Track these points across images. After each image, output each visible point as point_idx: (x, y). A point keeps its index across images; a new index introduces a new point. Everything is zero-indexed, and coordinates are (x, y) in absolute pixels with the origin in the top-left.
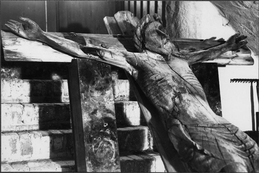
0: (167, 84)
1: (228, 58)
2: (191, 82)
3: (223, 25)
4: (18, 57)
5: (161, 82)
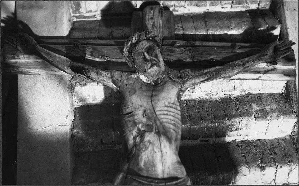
0: (133, 120)
1: (259, 72)
2: (162, 119)
3: (294, 10)
4: (15, 71)
5: (129, 117)
